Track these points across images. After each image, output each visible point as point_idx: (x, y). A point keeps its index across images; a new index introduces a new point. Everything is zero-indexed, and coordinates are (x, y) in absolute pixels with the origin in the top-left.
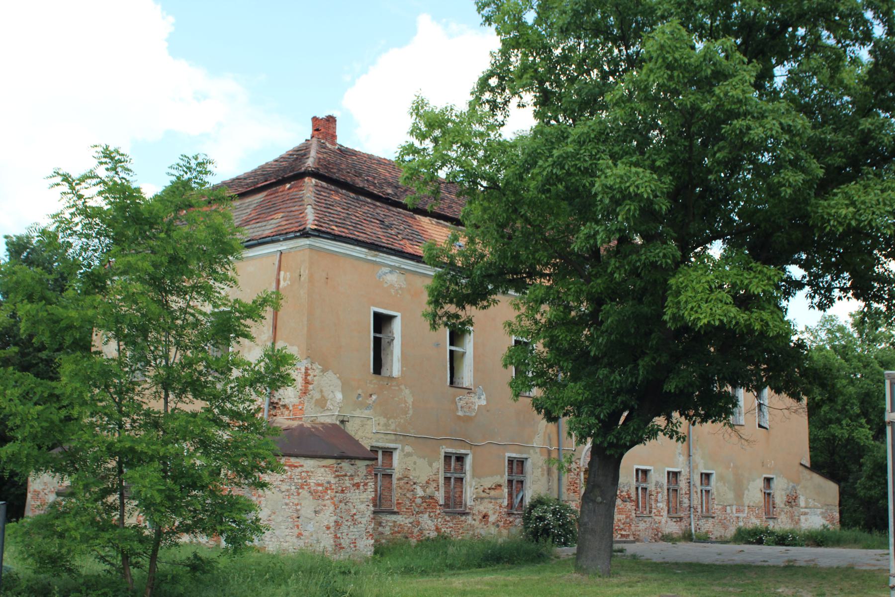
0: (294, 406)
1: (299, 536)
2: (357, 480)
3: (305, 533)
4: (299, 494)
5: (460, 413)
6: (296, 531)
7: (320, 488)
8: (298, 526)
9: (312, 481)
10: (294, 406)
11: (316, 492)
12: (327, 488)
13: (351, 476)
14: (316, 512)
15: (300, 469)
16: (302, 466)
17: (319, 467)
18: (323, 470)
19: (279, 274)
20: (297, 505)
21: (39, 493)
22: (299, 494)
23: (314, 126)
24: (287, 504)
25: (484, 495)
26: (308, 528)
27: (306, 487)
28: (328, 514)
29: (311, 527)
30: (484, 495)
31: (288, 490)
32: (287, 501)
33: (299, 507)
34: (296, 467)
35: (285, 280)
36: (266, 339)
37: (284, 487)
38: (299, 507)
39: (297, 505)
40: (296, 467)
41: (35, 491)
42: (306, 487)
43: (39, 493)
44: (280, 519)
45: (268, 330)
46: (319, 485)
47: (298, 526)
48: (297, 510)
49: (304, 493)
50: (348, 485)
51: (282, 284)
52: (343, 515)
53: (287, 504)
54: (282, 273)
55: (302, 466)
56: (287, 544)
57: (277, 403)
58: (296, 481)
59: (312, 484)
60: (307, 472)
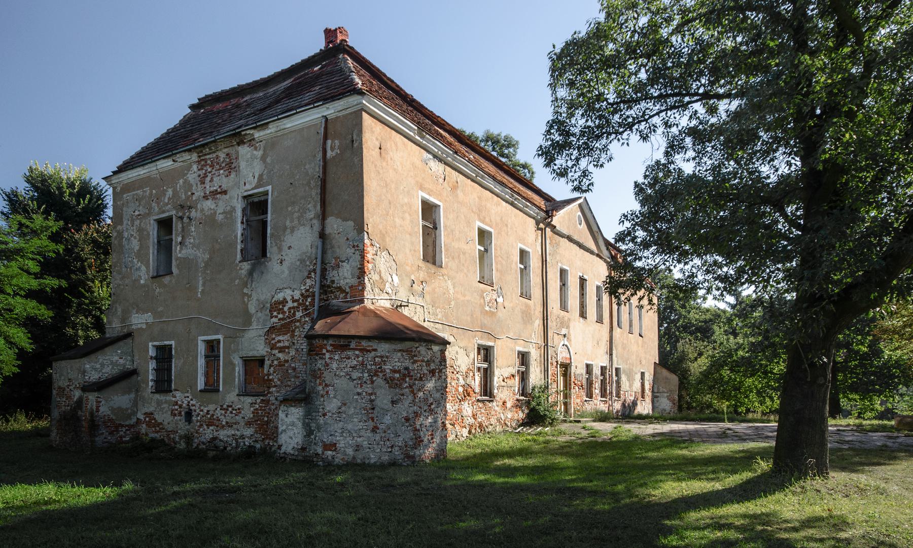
0: (351, 287)
1: (375, 430)
2: (433, 366)
3: (382, 426)
4: (372, 382)
5: (487, 308)
6: (371, 424)
7: (397, 375)
8: (373, 419)
9: (388, 367)
10: (351, 287)
11: (392, 379)
12: (404, 375)
13: (428, 361)
14: (393, 402)
15: (373, 353)
16: (375, 350)
17: (395, 350)
18: (399, 354)
19: (325, 143)
20: (371, 394)
21: (64, 389)
22: (372, 382)
23: (326, 38)
24: (359, 394)
25: (503, 384)
26: (385, 421)
27: (381, 375)
28: (406, 403)
29: (387, 420)
30: (503, 384)
31: (360, 378)
32: (359, 390)
33: (373, 397)
34: (369, 351)
35: (332, 149)
36: (312, 216)
37: (355, 375)
38: (373, 397)
39: (371, 394)
40: (369, 351)
41: (60, 388)
42: (381, 375)
43: (64, 389)
44: (352, 411)
45: (315, 207)
46: (395, 371)
47: (373, 419)
48: (372, 401)
49: (379, 381)
50: (426, 372)
51: (329, 154)
52: (422, 405)
53: (359, 394)
54: (329, 142)
55: (375, 350)
56: (361, 439)
57: (329, 286)
58: (369, 367)
59: (388, 371)
60: (382, 357)
